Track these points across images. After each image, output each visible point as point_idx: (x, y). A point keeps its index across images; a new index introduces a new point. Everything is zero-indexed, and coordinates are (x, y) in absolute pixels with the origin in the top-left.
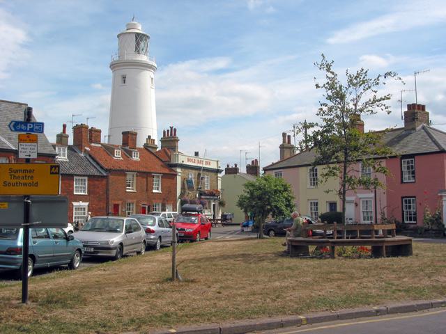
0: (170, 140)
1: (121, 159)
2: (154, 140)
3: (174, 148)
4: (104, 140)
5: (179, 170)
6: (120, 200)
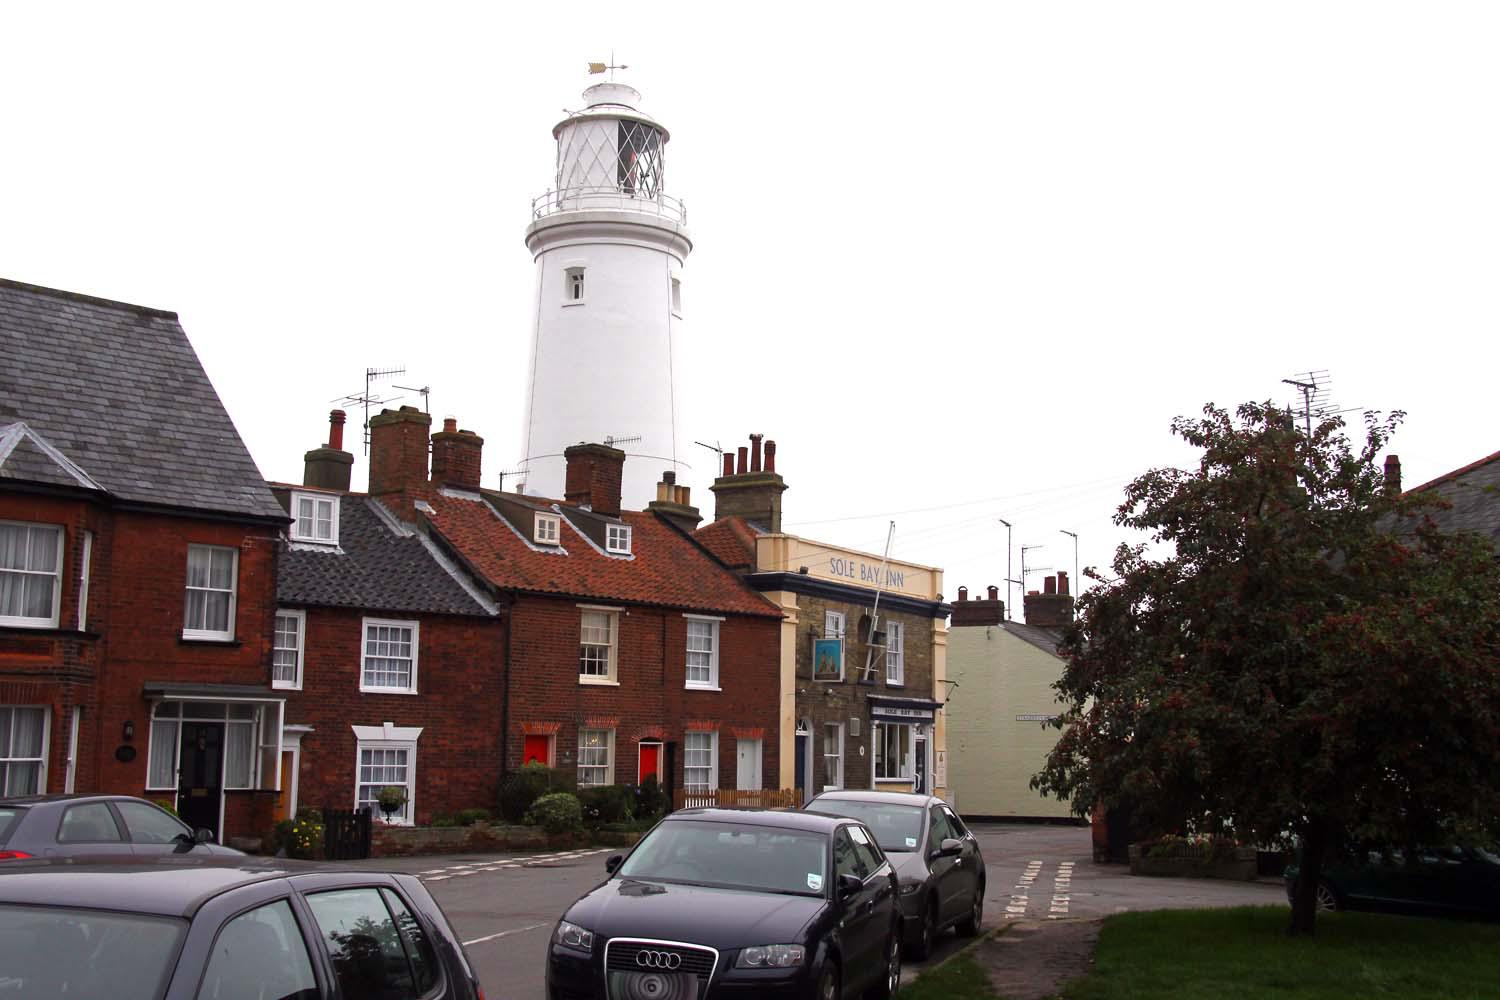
0: (752, 484)
1: (562, 551)
2: (686, 490)
3: (769, 519)
4: (499, 470)
5: (787, 600)
6: (555, 718)
